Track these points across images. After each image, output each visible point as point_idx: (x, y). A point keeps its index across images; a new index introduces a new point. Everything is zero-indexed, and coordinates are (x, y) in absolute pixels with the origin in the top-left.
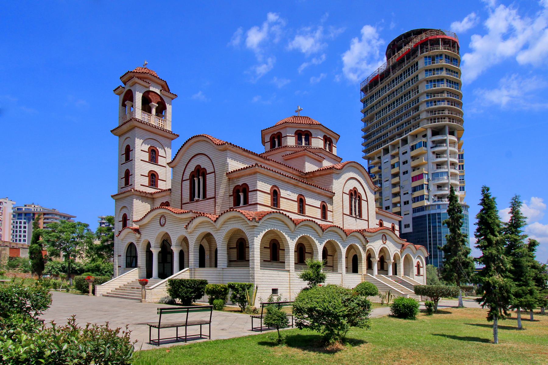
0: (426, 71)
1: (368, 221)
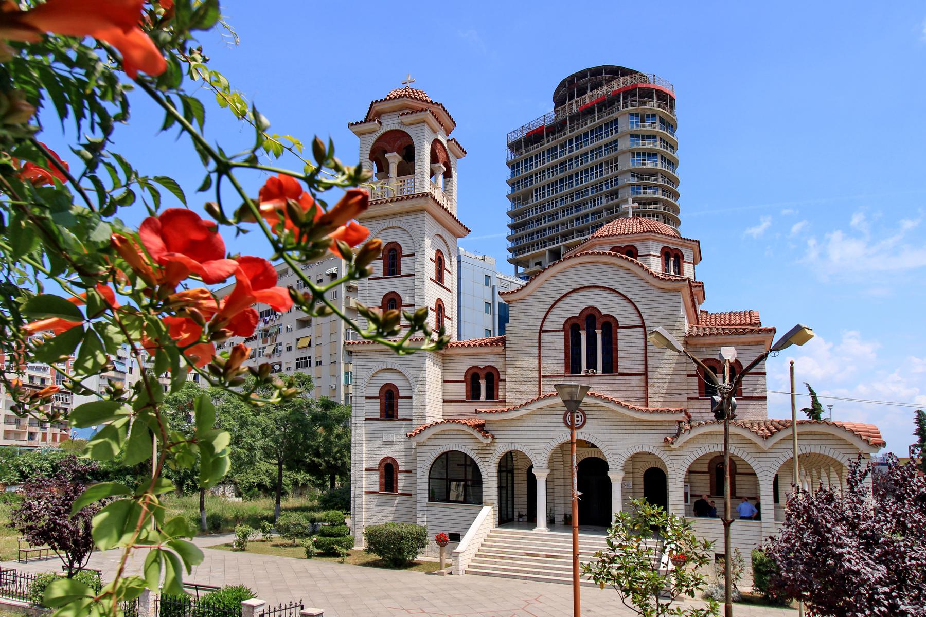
0: (632, 136)
1: (645, 374)
